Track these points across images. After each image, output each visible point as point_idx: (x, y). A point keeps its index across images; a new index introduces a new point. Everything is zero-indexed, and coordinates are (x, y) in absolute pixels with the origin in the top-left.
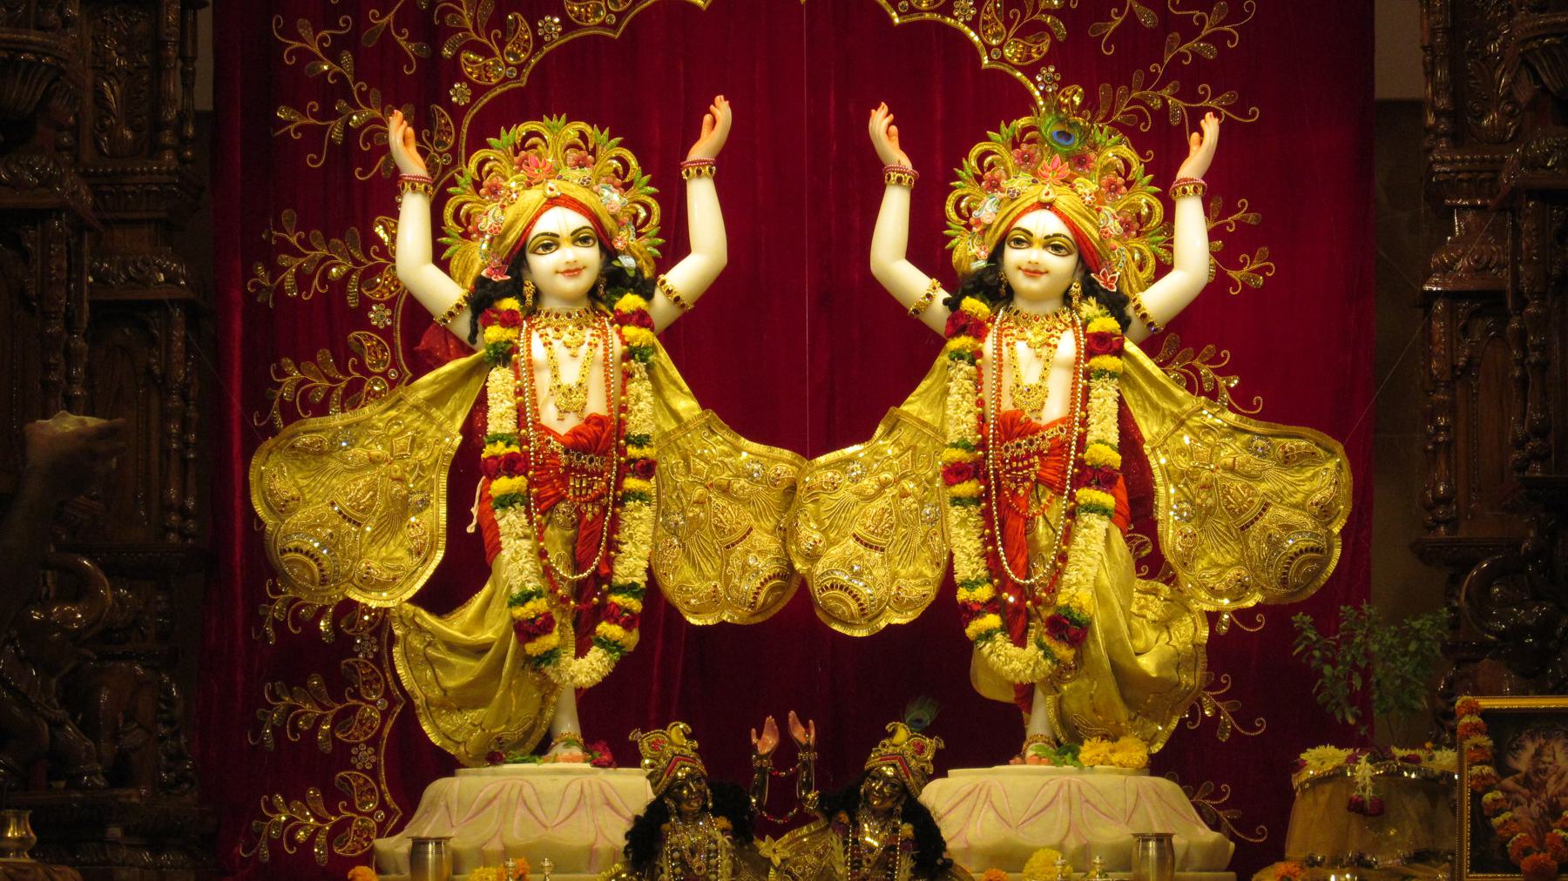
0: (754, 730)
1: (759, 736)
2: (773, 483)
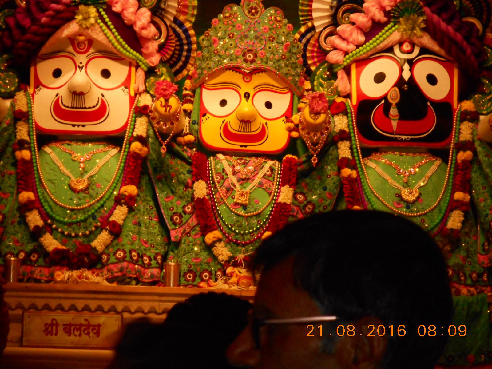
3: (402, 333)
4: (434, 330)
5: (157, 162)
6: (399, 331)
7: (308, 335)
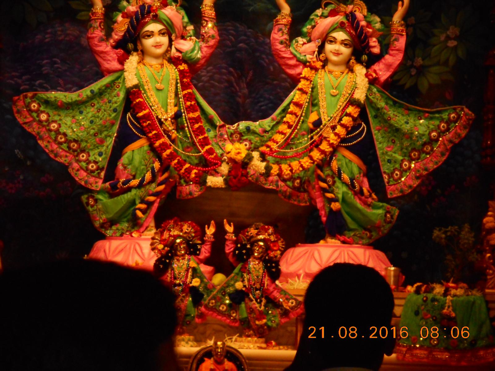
0: (206, 226)
1: (208, 228)
2: (102, 100)
3: (466, 335)
4: (355, 332)
5: (413, 176)
6: (401, 333)
7: (310, 337)
